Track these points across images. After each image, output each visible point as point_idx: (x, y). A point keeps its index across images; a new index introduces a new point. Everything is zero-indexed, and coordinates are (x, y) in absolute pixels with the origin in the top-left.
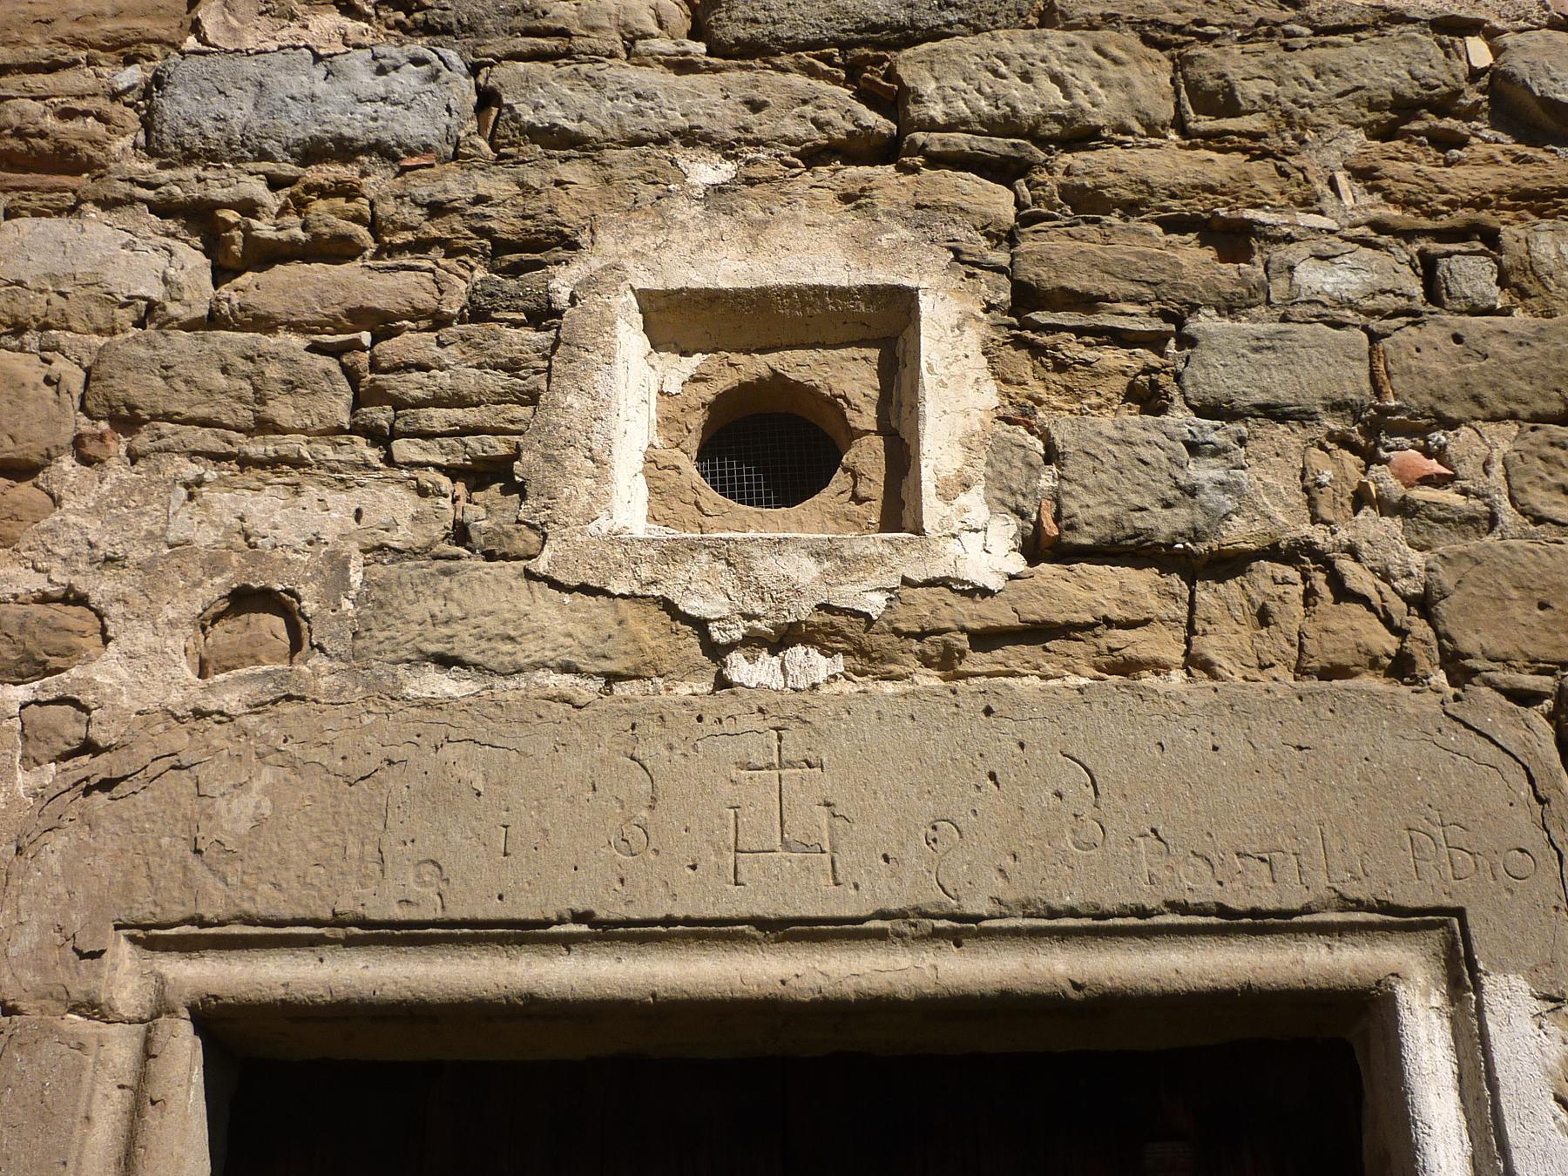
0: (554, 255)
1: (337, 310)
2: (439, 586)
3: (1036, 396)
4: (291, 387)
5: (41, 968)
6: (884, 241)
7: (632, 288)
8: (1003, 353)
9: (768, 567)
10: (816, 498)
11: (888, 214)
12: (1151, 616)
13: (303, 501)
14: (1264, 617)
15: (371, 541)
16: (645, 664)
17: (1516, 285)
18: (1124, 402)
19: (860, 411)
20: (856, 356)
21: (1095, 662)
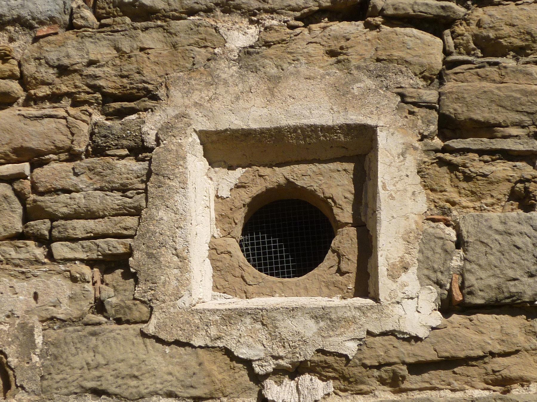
0: (143, 104)
1: (6, 148)
2: (90, 344)
3: (452, 200)
6: (356, 89)
7: (195, 131)
8: (431, 171)
10: (315, 271)
11: (358, 68)
12: (519, 348)
16: (216, 390)
18: (508, 201)
19: (342, 209)
20: (340, 169)
21: (484, 379)
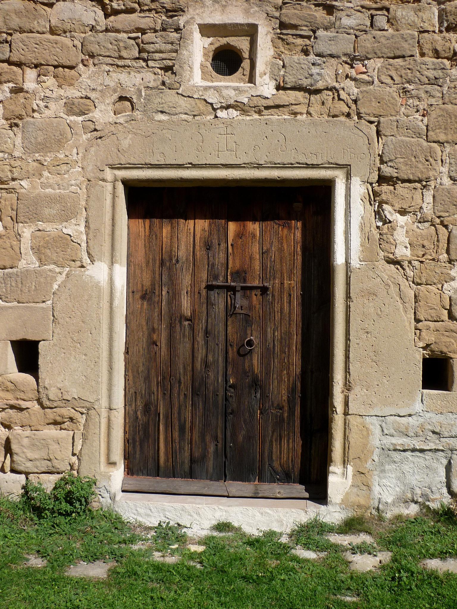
4: (126, 48)
5: (94, 173)
6: (252, 11)
9: (225, 92)
10: (235, 74)
11: (253, 3)
13: (131, 76)
14: (323, 103)
15: (146, 86)
17: (391, 22)
